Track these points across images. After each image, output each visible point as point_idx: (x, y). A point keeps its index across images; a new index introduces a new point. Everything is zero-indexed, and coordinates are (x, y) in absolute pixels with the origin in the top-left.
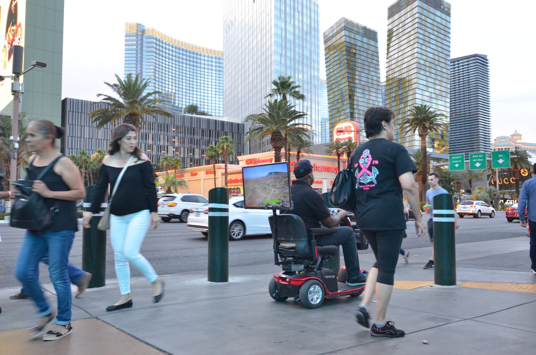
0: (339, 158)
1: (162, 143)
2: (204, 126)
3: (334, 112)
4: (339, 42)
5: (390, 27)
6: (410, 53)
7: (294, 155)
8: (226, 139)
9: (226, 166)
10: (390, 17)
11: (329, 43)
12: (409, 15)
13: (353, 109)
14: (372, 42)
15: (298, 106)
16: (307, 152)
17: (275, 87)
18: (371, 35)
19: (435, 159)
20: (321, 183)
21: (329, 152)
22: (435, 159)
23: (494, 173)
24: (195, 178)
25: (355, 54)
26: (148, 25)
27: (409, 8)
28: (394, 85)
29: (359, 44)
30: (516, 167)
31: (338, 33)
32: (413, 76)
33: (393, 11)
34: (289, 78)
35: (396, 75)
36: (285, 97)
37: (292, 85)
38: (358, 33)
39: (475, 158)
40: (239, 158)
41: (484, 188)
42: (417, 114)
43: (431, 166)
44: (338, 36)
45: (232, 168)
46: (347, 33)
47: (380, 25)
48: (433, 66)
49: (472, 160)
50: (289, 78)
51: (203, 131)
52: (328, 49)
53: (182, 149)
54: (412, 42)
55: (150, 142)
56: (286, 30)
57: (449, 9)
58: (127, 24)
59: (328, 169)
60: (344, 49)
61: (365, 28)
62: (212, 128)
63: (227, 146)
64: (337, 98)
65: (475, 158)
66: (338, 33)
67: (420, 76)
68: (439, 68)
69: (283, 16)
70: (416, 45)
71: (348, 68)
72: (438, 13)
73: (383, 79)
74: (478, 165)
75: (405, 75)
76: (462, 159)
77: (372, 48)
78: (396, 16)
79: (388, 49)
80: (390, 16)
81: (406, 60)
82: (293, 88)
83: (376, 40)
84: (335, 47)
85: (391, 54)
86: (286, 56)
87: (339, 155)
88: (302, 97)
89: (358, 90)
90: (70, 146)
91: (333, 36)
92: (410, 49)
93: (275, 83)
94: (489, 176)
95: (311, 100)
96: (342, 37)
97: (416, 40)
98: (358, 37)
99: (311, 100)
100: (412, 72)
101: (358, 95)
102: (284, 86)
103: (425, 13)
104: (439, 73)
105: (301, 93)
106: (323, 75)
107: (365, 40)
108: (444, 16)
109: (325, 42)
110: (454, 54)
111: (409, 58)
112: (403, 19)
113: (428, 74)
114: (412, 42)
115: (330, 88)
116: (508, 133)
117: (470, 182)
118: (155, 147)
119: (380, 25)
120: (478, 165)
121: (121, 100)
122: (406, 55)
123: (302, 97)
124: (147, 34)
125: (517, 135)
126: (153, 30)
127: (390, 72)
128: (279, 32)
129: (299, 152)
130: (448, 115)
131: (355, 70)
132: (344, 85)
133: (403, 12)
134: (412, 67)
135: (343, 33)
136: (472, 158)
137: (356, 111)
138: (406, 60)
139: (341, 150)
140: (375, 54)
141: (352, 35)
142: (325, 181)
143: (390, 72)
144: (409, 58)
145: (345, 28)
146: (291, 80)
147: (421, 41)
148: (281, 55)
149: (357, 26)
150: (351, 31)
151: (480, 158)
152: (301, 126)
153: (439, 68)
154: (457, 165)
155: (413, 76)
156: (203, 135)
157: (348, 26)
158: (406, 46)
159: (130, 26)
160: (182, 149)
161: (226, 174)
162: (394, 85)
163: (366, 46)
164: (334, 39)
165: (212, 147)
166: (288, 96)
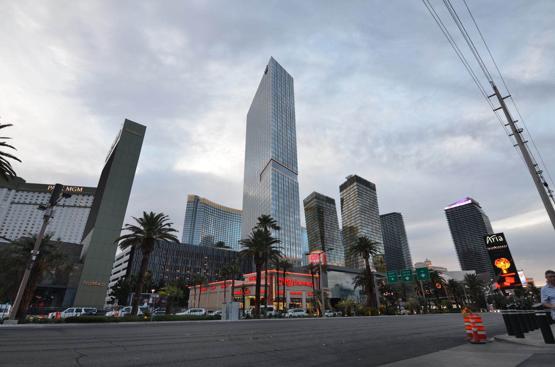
0: (313, 276)
1: (197, 267)
2: (226, 255)
3: (312, 247)
4: (313, 205)
5: (342, 197)
6: (355, 211)
7: (281, 273)
8: (234, 261)
9: (233, 282)
10: (341, 191)
11: (307, 206)
12: (352, 190)
13: (324, 245)
14: (332, 206)
15: (273, 234)
16: (291, 271)
17: (260, 222)
18: (332, 201)
19: (377, 276)
20: (301, 294)
21: (306, 272)
22: (377, 276)
23: (420, 285)
24: (214, 291)
25: (323, 212)
26: (201, 196)
27: (351, 186)
28: (348, 230)
29: (325, 206)
30: (433, 281)
31: (312, 200)
32: (359, 225)
33: (343, 188)
34: (269, 216)
35: (348, 224)
36: (266, 229)
37: (272, 220)
38: (323, 200)
39: (404, 274)
40: (245, 276)
41: (415, 296)
42: (360, 242)
43: (375, 280)
44: (312, 202)
45: (238, 283)
46: (317, 200)
47: (336, 196)
48: (370, 219)
49: (402, 275)
50: (269, 216)
51: (225, 258)
52: (306, 210)
53: (210, 271)
54: (355, 205)
55: (189, 266)
56: (279, 196)
57: (375, 187)
58: (189, 196)
59: (305, 284)
60: (316, 209)
61: (327, 198)
62: (231, 256)
63: (235, 267)
64: (313, 238)
65: (404, 274)
66: (312, 200)
67: (362, 225)
68: (373, 220)
69: (277, 188)
70: (358, 206)
71: (319, 220)
72: (368, 189)
73: (341, 227)
74: (407, 278)
75: (353, 224)
76: (395, 274)
77: (333, 209)
78: (345, 191)
79: (342, 209)
80: (341, 191)
81: (353, 215)
82: (272, 222)
83: (334, 204)
84: (310, 208)
85: (344, 212)
86: (279, 211)
87: (313, 273)
88: (278, 228)
89: (326, 233)
90: (134, 269)
91: (309, 202)
92: (354, 208)
93: (259, 219)
94: (416, 289)
95: (285, 229)
96: (314, 203)
97: (358, 204)
98: (324, 203)
99: (285, 229)
100: (357, 222)
101: (326, 236)
102: (265, 221)
103: (361, 189)
104: (374, 223)
105: (277, 225)
106: (303, 223)
107: (328, 204)
108: (372, 191)
109: (305, 205)
110: (381, 213)
111: (355, 214)
112: (349, 192)
113: (367, 223)
114: (355, 205)
115: (309, 233)
116: (423, 261)
117: (404, 293)
118: (192, 269)
119: (336, 196)
120: (407, 278)
121: (142, 228)
122: (353, 212)
123: (278, 228)
124: (200, 201)
125: (428, 261)
126: (204, 199)
127: (345, 222)
128: (275, 197)
129: (285, 272)
130: (382, 242)
131: (323, 221)
132: (317, 229)
133: (348, 188)
134: (357, 219)
135: (315, 200)
136: (402, 274)
137: (326, 246)
138: (353, 215)
139: (314, 270)
140: (335, 212)
141: (320, 201)
142: (304, 293)
143: (345, 222)
144: (355, 214)
145: (316, 197)
146: (271, 217)
147: (361, 204)
148: (276, 211)
149: (323, 196)
150: (319, 199)
151: (408, 273)
152: (275, 249)
153: (373, 220)
154: (393, 279)
155: (359, 225)
156: (225, 261)
157: (317, 196)
158: (352, 207)
159: (190, 197)
160: (210, 271)
161: (233, 288)
162: (348, 230)
163: (329, 207)
164: (310, 204)
165: (224, 268)
166: (268, 229)
